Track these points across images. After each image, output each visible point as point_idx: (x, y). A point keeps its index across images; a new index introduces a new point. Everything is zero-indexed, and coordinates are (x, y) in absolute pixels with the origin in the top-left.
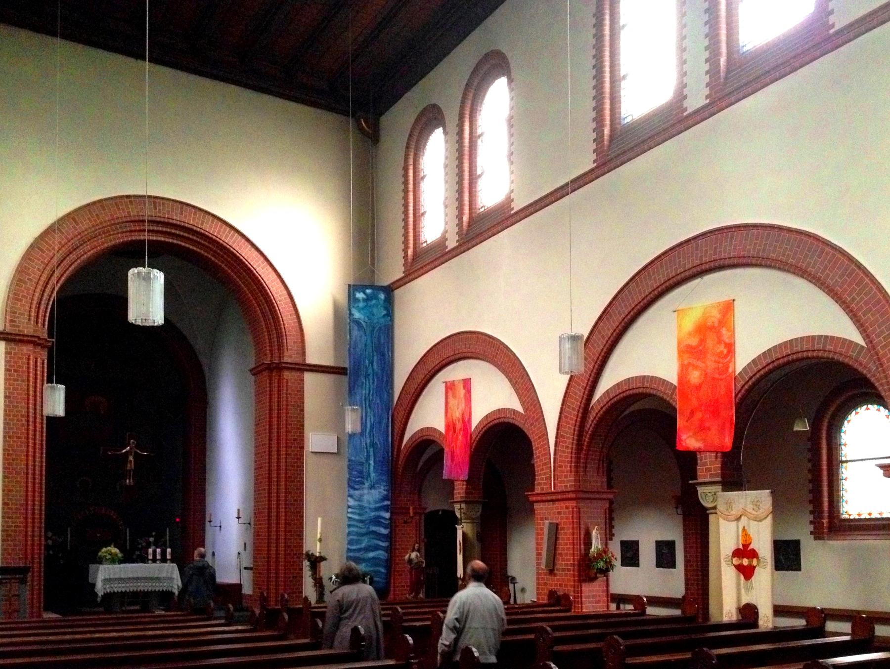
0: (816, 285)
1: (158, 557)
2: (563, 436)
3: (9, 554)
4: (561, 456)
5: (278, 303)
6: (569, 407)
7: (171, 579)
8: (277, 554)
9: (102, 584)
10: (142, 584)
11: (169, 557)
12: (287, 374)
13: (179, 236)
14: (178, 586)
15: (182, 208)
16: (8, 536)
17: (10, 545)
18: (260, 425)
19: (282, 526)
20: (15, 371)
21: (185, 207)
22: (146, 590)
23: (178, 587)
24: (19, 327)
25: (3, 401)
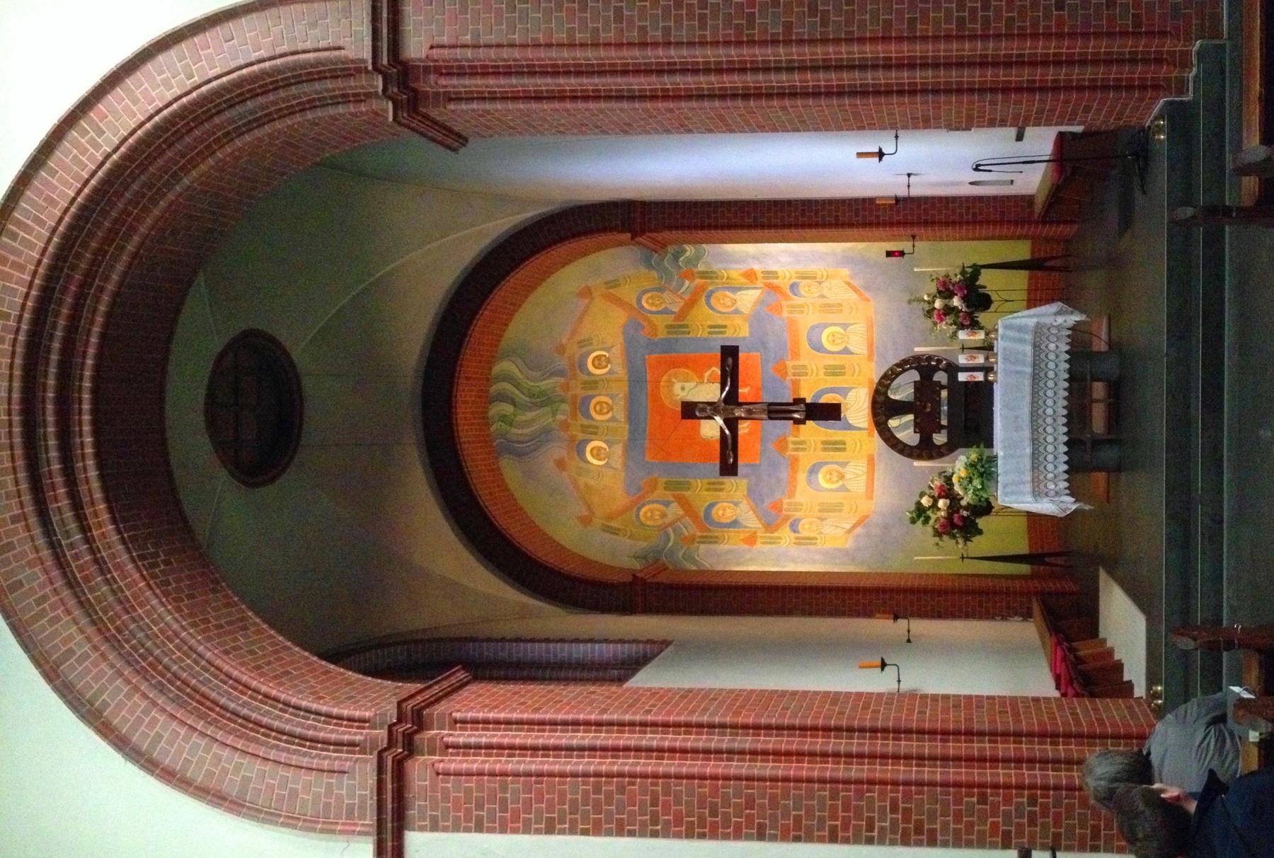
1: (980, 359)
3: (970, 826)
5: (197, 79)
7: (1039, 330)
8: (312, 105)
9: (1046, 500)
16: (919, 830)
17: (945, 825)
19: (893, 50)
20: (480, 806)
22: (1066, 394)
23: (1059, 313)
25: (561, 837)
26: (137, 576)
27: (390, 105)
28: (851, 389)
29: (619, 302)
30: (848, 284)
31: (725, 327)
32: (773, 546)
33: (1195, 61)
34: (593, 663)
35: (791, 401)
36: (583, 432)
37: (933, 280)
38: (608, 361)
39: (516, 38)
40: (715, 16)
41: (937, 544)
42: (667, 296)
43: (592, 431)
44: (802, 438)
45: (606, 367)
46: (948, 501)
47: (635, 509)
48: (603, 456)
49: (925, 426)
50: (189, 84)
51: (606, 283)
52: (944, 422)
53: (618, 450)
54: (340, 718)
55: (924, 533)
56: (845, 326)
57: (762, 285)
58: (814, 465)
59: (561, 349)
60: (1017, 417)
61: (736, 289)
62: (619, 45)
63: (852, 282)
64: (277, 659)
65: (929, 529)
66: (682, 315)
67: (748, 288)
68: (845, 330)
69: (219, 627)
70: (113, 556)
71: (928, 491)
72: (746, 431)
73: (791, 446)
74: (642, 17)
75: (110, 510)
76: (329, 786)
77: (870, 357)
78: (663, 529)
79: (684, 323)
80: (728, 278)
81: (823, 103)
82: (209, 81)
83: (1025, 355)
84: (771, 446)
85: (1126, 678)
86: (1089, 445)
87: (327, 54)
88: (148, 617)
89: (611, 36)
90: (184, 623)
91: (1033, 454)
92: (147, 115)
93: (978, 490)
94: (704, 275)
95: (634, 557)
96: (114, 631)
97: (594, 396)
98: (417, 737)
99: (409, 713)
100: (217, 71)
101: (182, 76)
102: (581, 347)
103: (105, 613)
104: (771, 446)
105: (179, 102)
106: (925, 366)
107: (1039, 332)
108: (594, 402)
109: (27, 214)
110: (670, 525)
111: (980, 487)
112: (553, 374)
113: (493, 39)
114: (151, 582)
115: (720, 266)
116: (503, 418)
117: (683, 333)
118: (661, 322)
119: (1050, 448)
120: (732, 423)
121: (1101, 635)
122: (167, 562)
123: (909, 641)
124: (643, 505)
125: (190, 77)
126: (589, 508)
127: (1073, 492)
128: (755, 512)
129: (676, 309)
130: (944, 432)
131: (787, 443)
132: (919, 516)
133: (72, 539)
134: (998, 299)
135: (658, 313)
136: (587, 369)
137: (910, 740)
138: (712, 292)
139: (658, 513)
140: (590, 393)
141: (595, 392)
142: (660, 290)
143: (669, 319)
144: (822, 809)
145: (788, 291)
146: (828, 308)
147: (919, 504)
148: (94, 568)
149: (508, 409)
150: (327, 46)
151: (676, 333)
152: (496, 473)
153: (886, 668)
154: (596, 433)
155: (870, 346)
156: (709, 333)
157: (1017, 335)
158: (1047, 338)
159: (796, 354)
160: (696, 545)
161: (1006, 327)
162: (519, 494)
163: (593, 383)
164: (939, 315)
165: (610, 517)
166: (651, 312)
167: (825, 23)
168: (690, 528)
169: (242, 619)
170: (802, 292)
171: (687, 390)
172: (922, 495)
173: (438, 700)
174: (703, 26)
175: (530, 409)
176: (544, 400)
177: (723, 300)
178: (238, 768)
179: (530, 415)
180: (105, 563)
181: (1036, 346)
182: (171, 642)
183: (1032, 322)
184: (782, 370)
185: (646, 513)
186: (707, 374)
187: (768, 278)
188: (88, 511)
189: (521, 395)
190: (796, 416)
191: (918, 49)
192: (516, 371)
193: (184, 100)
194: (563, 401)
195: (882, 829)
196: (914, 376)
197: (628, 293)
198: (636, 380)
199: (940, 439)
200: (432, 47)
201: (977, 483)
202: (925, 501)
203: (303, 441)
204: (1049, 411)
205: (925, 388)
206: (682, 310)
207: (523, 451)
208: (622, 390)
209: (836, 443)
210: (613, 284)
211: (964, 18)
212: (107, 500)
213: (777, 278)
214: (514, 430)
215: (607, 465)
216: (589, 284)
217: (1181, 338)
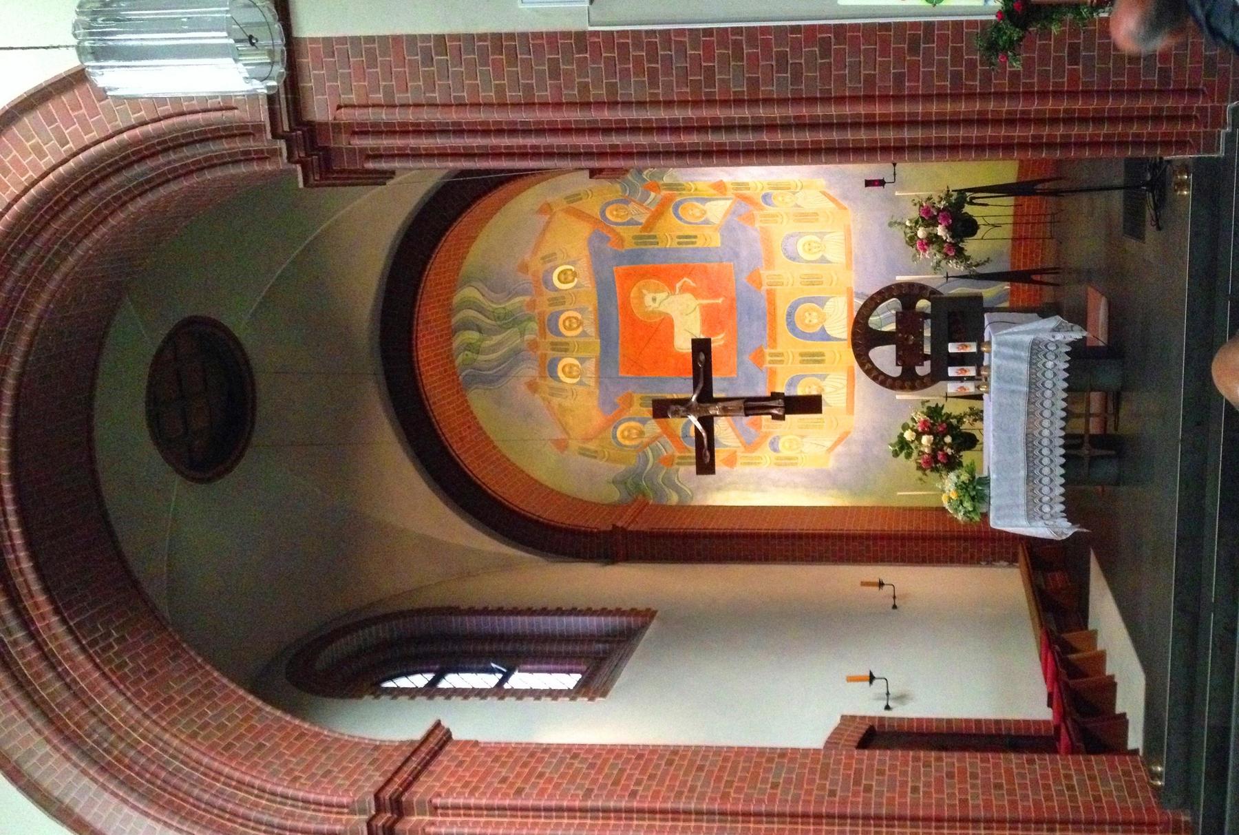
0: (50, 85)
9: (1041, 523)
10: (1046, 423)
11: (972, 348)
14: (1057, 329)
18: (444, 356)
23: (1057, 329)
26: (89, 666)
27: (299, 168)
28: (829, 298)
29: (580, 215)
30: (824, 193)
31: (695, 237)
32: (753, 467)
33: (1229, 119)
34: (577, 635)
35: (768, 394)
36: (553, 349)
37: (915, 205)
38: (575, 274)
39: (437, 96)
40: (667, 73)
41: (921, 479)
42: (632, 207)
43: (563, 348)
44: (779, 350)
45: (573, 281)
46: (932, 437)
47: (611, 429)
48: (574, 374)
49: (909, 356)
50: (64, 151)
51: (567, 198)
52: (927, 350)
53: (591, 365)
55: (906, 466)
56: (821, 235)
57: (733, 196)
58: (792, 378)
59: (524, 268)
60: (1010, 438)
61: (704, 200)
63: (827, 191)
64: (249, 730)
65: (912, 463)
66: (649, 226)
67: (717, 199)
68: (821, 238)
69: (184, 703)
70: (62, 647)
71: (911, 424)
72: (722, 343)
73: (768, 358)
74: (582, 71)
75: (52, 600)
77: (848, 265)
78: (640, 449)
79: (652, 233)
80: (696, 189)
82: (86, 148)
83: (1021, 374)
84: (747, 358)
85: (1119, 709)
86: (1086, 461)
87: (219, 114)
88: (107, 706)
89: (548, 95)
90: (146, 710)
91: (1028, 476)
92: (22, 188)
93: (969, 512)
94: (670, 187)
95: (613, 482)
96: (73, 727)
97: (562, 312)
98: (398, 827)
99: (387, 802)
100: (95, 135)
101: (54, 141)
102: (545, 263)
103: (62, 709)
104: (747, 358)
105: (56, 173)
106: (907, 293)
107: (1036, 349)
108: (563, 317)
110: (648, 444)
111: (971, 509)
112: (517, 294)
113: (409, 97)
114: (106, 670)
115: (687, 178)
116: (469, 347)
117: (651, 243)
118: (628, 233)
119: (1046, 471)
120: (707, 422)
121: (1091, 627)
122: (120, 640)
123: (895, 607)
124: (620, 423)
125: (63, 143)
126: (565, 430)
127: (1071, 513)
128: (733, 429)
129: (643, 220)
130: (927, 364)
131: (763, 355)
132: (902, 449)
133: (15, 637)
134: (983, 222)
135: (623, 224)
136: (553, 285)
137: (904, 826)
138: (681, 202)
139: (635, 431)
140: (558, 308)
141: (561, 308)
142: (626, 201)
143: (636, 230)
145: (761, 201)
146: (805, 217)
147: (901, 436)
148: (42, 665)
149: (473, 336)
150: (217, 106)
151: (645, 243)
152: (466, 411)
153: (875, 682)
154: (566, 350)
155: (849, 253)
156: (679, 243)
157: (1011, 352)
158: (1045, 356)
159: (770, 263)
160: (676, 467)
161: (999, 344)
162: (489, 427)
163: (559, 300)
164: (922, 244)
165: (587, 439)
166: (617, 224)
167: (797, 78)
168: (667, 447)
169: (209, 684)
170: (775, 202)
171: (658, 301)
172: (905, 427)
173: (416, 776)
174: (653, 82)
175: (496, 333)
176: (509, 321)
177: (693, 211)
179: (496, 339)
180: (54, 655)
181: (1032, 364)
182: (135, 731)
183: (1028, 339)
184: (755, 279)
185: (623, 432)
186: (678, 285)
187: (740, 189)
188: (28, 603)
189: (488, 321)
190: (775, 411)
191: (878, 109)
192: (478, 295)
193: (61, 169)
194: (530, 319)
196: (893, 304)
197: (592, 206)
198: (604, 289)
199: (924, 369)
200: (339, 107)
201: (968, 505)
202: (908, 435)
203: (254, 440)
204: (1046, 433)
205: (907, 319)
206: (648, 221)
207: (491, 378)
208: (590, 302)
209: (813, 355)
210: (575, 198)
211: (960, 73)
212: (46, 590)
213: (749, 189)
214: (481, 357)
215: (580, 383)
216: (549, 199)
217: (1198, 424)
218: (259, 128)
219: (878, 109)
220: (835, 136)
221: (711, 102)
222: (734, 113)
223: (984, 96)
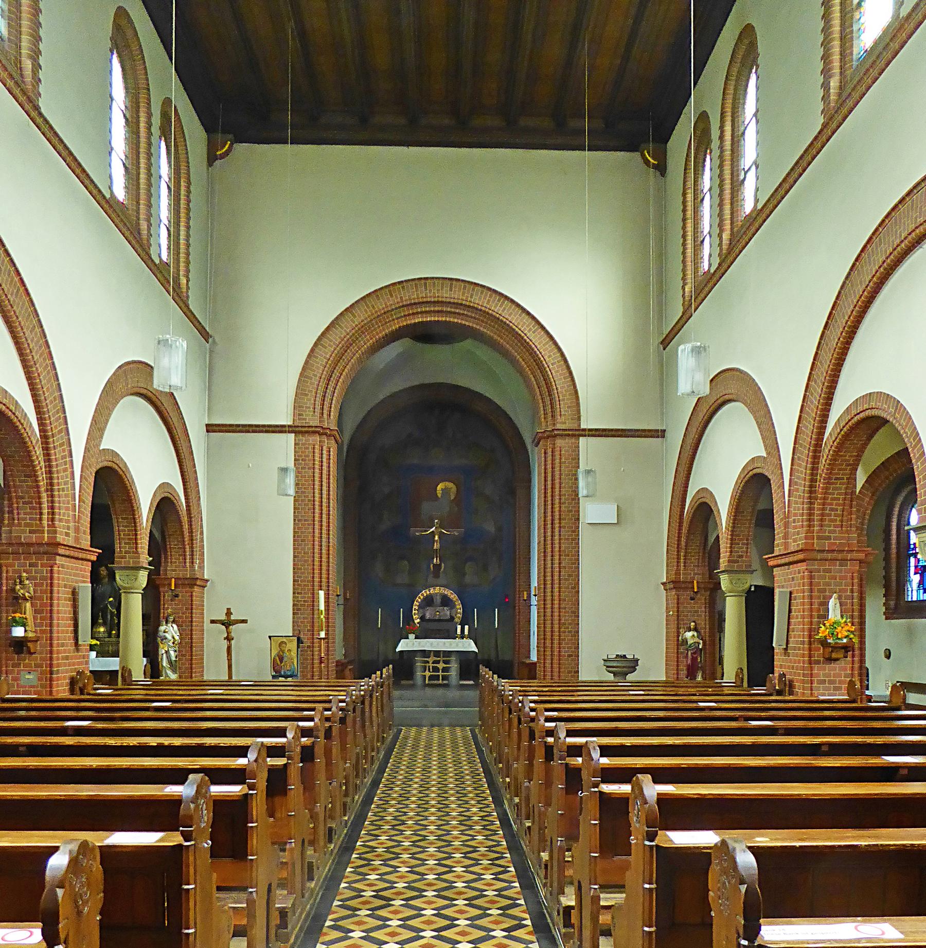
2: (796, 484)
4: (66, 483)
6: (801, 445)
12: (559, 442)
13: (450, 312)
15: (451, 284)
21: (454, 283)
24: (305, 419)
54: (331, 407)
62: (560, 511)
76: (309, 408)
81: (54, 463)
100: (554, 374)
109: (507, 305)
144: (825, 577)
167: (566, 580)
178: (315, 376)
191: (556, 602)
195: (298, 597)
218: (554, 424)
219: (556, 602)
220: (550, 502)
221: (560, 555)
222: (557, 561)
223: (559, 632)
